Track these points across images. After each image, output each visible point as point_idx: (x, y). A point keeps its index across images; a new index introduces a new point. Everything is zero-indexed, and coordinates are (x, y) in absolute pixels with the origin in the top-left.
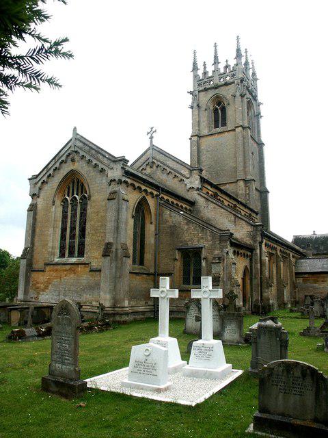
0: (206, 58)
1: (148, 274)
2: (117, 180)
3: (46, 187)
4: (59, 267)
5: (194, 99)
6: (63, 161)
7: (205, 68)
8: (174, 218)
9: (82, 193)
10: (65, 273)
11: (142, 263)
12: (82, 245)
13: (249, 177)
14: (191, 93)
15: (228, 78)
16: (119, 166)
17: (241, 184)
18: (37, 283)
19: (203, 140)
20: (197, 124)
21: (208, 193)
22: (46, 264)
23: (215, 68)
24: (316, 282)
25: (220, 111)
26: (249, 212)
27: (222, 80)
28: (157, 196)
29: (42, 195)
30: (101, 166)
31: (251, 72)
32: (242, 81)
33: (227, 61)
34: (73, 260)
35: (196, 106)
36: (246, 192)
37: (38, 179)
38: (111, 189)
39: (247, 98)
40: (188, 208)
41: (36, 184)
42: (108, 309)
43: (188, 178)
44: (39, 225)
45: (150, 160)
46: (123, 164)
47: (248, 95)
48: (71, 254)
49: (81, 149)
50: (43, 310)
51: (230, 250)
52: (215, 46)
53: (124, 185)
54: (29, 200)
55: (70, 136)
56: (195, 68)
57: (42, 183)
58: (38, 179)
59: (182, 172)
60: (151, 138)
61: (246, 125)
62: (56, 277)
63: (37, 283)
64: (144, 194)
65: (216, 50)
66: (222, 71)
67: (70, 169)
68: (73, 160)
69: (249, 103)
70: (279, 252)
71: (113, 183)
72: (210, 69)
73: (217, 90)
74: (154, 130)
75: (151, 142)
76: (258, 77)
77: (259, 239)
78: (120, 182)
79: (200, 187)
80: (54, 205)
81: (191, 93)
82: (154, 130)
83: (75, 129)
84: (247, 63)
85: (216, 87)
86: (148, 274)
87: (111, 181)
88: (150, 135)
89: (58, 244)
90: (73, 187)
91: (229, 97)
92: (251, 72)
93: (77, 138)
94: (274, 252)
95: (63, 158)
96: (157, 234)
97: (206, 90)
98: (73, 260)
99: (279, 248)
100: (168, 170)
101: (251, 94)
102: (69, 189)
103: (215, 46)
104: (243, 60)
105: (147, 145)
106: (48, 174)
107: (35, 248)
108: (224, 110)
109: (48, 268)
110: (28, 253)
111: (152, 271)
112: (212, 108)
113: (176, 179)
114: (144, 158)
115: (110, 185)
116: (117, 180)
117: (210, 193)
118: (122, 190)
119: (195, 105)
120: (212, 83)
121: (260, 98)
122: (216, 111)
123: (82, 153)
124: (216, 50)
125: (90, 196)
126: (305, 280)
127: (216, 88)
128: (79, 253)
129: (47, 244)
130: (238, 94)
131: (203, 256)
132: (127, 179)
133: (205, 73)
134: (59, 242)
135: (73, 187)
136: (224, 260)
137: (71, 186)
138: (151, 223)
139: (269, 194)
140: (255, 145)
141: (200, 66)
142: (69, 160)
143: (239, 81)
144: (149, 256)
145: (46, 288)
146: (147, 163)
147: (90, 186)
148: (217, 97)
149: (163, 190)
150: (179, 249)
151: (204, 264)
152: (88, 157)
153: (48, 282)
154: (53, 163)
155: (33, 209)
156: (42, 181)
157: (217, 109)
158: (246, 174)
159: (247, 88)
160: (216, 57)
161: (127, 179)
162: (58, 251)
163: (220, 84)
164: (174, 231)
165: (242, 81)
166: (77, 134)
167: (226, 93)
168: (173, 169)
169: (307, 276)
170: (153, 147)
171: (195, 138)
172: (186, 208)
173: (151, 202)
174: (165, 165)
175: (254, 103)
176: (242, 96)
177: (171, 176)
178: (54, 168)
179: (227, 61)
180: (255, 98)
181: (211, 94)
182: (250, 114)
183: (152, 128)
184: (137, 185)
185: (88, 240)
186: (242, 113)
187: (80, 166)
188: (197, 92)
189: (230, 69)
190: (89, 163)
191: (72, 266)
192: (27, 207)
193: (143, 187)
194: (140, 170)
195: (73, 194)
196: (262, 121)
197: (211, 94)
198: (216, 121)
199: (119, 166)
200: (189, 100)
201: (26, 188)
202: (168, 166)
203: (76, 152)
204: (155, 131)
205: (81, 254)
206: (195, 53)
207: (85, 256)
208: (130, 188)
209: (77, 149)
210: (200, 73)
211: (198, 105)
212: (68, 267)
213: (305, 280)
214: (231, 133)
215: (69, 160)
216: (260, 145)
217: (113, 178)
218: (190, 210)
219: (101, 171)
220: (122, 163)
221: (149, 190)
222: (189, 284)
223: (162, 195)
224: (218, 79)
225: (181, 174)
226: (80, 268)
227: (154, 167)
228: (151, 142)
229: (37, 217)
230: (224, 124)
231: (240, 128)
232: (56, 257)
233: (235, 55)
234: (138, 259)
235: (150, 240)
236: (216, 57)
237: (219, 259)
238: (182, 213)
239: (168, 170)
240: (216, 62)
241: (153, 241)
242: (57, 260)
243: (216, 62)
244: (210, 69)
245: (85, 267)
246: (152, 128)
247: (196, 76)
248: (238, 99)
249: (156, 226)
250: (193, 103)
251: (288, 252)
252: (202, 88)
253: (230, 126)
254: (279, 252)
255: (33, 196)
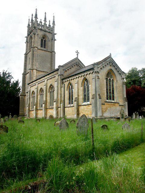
4: (110, 103)
7: (50, 23)
12: (113, 96)
52: (45, 14)
62: (109, 107)
65: (45, 15)
74: (77, 52)
82: (77, 52)
93: (110, 57)
103: (45, 14)
124: (45, 15)
127: (45, 32)
128: (113, 99)
141: (48, 20)
145: (106, 111)
153: (106, 109)
160: (45, 18)
170: (77, 58)
183: (76, 52)
204: (77, 51)
206: (36, 10)
212: (113, 104)
226: (116, 104)
233: (44, 20)
236: (45, 18)
244: (43, 22)
246: (76, 52)
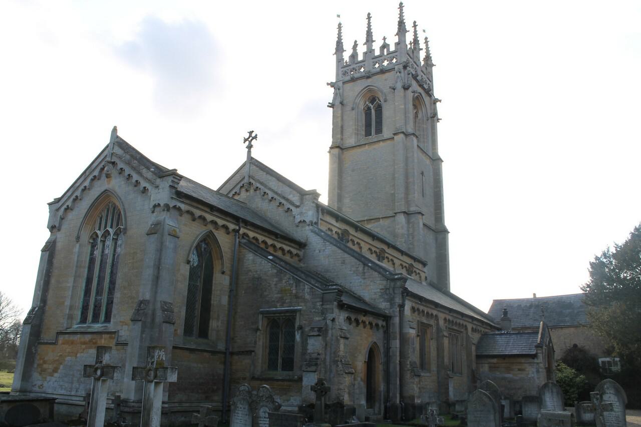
0: (354, 35)
1: (214, 353)
2: (162, 205)
3: (71, 216)
5: (335, 94)
6: (95, 177)
8: (255, 264)
9: (118, 225)
10: (84, 346)
11: (204, 332)
13: (413, 209)
14: (332, 85)
15: (386, 63)
16: (165, 184)
17: (401, 218)
18: (45, 362)
19: (348, 154)
20: (339, 129)
21: (331, 230)
22: (60, 333)
23: (368, 48)
24: (509, 370)
25: (373, 111)
26: (409, 261)
27: (377, 65)
28: (236, 231)
29: (65, 227)
30: (143, 184)
31: (422, 55)
32: (405, 67)
33: (384, 39)
34: (97, 327)
35: (338, 105)
36: (408, 231)
37: (60, 203)
38: (152, 219)
39: (414, 92)
40: (294, 251)
41: (58, 210)
42: (133, 404)
43: (297, 207)
44: (55, 272)
45: (246, 180)
46: (173, 181)
47: (415, 86)
48: (96, 319)
49: (120, 158)
50: (35, 404)
51: (341, 317)
52: (369, 18)
53: (175, 213)
54: (46, 235)
55: (106, 140)
56: (339, 48)
57: (66, 209)
58: (60, 203)
59: (290, 197)
60: (250, 147)
61: (410, 130)
63: (45, 362)
64: (211, 227)
66: (377, 53)
67: (103, 189)
68: (108, 176)
69: (418, 102)
70: (441, 322)
71: (157, 209)
72: (362, 49)
73: (369, 80)
74: (253, 135)
75: (249, 152)
76: (434, 62)
77: (398, 300)
78: (167, 208)
79: (315, 220)
80: (77, 242)
81: (332, 85)
82: (253, 135)
83: (115, 130)
84: (416, 41)
85: (368, 76)
86: (214, 353)
87: (155, 206)
88: (247, 143)
89: (79, 303)
90: (107, 216)
91: (387, 90)
92: (422, 55)
94: (432, 322)
95: (96, 173)
96: (233, 293)
97: (353, 80)
98: (97, 327)
99: (441, 316)
100: (271, 194)
101: (421, 86)
102: (101, 219)
103: (369, 18)
104: (409, 38)
105: (244, 159)
106: (74, 197)
107: (47, 308)
108: (379, 109)
109: (61, 339)
110: (37, 318)
111: (221, 346)
112: (362, 107)
113: (280, 209)
114: (238, 178)
115: (153, 212)
116: (162, 205)
117: (335, 230)
118: (170, 221)
119: (337, 103)
120: (362, 70)
121: (437, 93)
122: (368, 111)
123: (121, 165)
125: (125, 229)
126: (493, 368)
127: (368, 77)
129: (63, 303)
130: (399, 85)
131: (297, 325)
132: (179, 204)
133: (354, 56)
134: (82, 300)
135: (107, 216)
136: (327, 330)
137: (104, 215)
138: (223, 273)
139: (449, 234)
140: (428, 162)
142: (104, 176)
143: (401, 67)
144: (216, 324)
145: (55, 370)
146: (241, 184)
147: (128, 214)
148: (370, 91)
149: (246, 223)
150: (262, 313)
151: (298, 337)
152: (128, 171)
154: (82, 179)
155: (49, 250)
156: (65, 206)
157: (369, 109)
158: (408, 202)
159: (415, 77)
160: (369, 34)
161: (179, 204)
162: (79, 313)
163: (374, 71)
164: (257, 285)
165: (405, 67)
166: (118, 137)
167: (381, 83)
168: (276, 193)
169: (495, 360)
170: (251, 161)
171: (336, 151)
172: (289, 252)
173: (223, 239)
174: (266, 186)
175: (426, 99)
176: (406, 88)
177: (274, 204)
178: (82, 187)
179: (384, 39)
180: (429, 92)
181: (360, 85)
182: (420, 116)
184: (198, 213)
185: (117, 296)
186: (405, 113)
187: (117, 184)
188: (340, 84)
189: (388, 50)
190: (128, 179)
191: (95, 336)
192: (42, 244)
193: (209, 217)
194: (230, 195)
195: (106, 227)
196: (439, 126)
197: (360, 85)
198: (368, 125)
199: (165, 184)
200: (329, 94)
201: (44, 215)
202: (270, 189)
203: (113, 163)
204: (255, 137)
205: (108, 319)
207: (112, 320)
208: (186, 218)
209: (114, 159)
210: (346, 56)
211: (342, 103)
212: (88, 338)
213: (493, 368)
214: (389, 142)
215: (104, 176)
216: (436, 161)
217: (157, 202)
218: (297, 255)
219: (143, 192)
220: (170, 179)
221: (221, 222)
222: (276, 369)
223: (242, 231)
224: (372, 64)
225: (287, 200)
227: (252, 191)
228: (249, 152)
229: (55, 261)
230: (379, 130)
231: (402, 136)
232: (74, 322)
234: (196, 330)
235: (220, 298)
236: (369, 34)
237: (320, 329)
238: (270, 257)
239: (271, 194)
240: (369, 39)
241: (225, 300)
242: (75, 327)
243: (369, 39)
245: (111, 338)
246: (251, 133)
247: (340, 60)
248: (400, 91)
249: (231, 279)
250: (334, 99)
251: (465, 323)
252: (348, 78)
253: (387, 132)
254: (441, 322)
255: (52, 228)
